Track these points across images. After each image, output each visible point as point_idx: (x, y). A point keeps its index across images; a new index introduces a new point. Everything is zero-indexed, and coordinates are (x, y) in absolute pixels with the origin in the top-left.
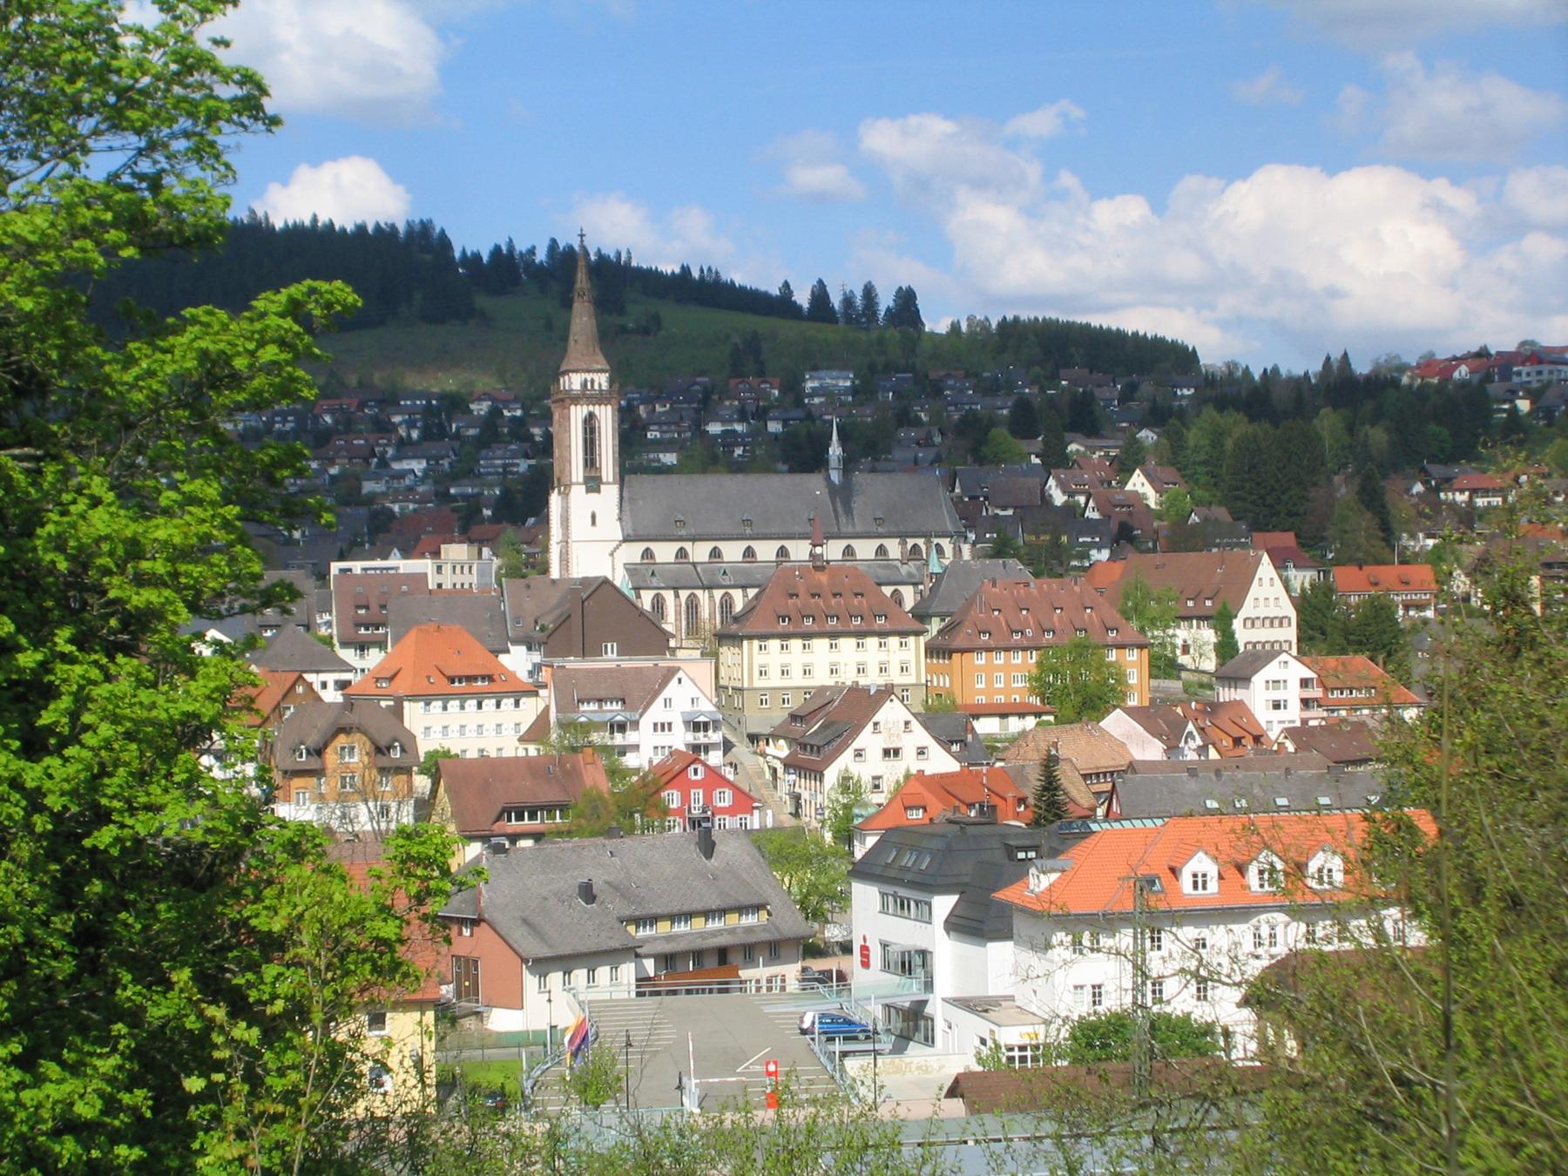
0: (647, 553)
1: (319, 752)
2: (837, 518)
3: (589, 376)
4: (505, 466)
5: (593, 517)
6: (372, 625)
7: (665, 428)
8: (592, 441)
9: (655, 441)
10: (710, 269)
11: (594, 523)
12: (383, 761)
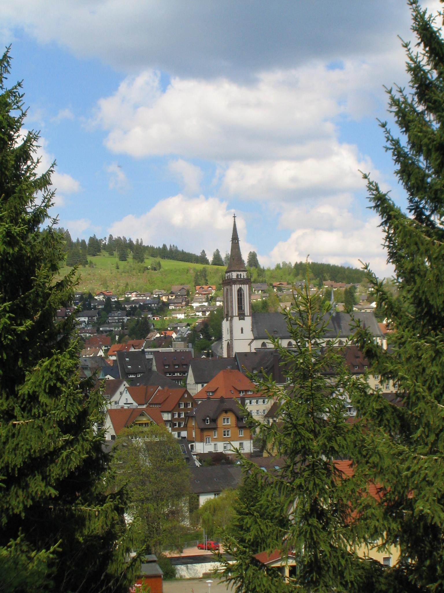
0: (264, 344)
1: (214, 420)
2: (335, 329)
3: (239, 273)
4: (119, 319)
5: (242, 329)
6: (172, 372)
7: (176, 305)
8: (241, 299)
9: (173, 310)
10: (173, 246)
11: (242, 332)
12: (241, 424)
